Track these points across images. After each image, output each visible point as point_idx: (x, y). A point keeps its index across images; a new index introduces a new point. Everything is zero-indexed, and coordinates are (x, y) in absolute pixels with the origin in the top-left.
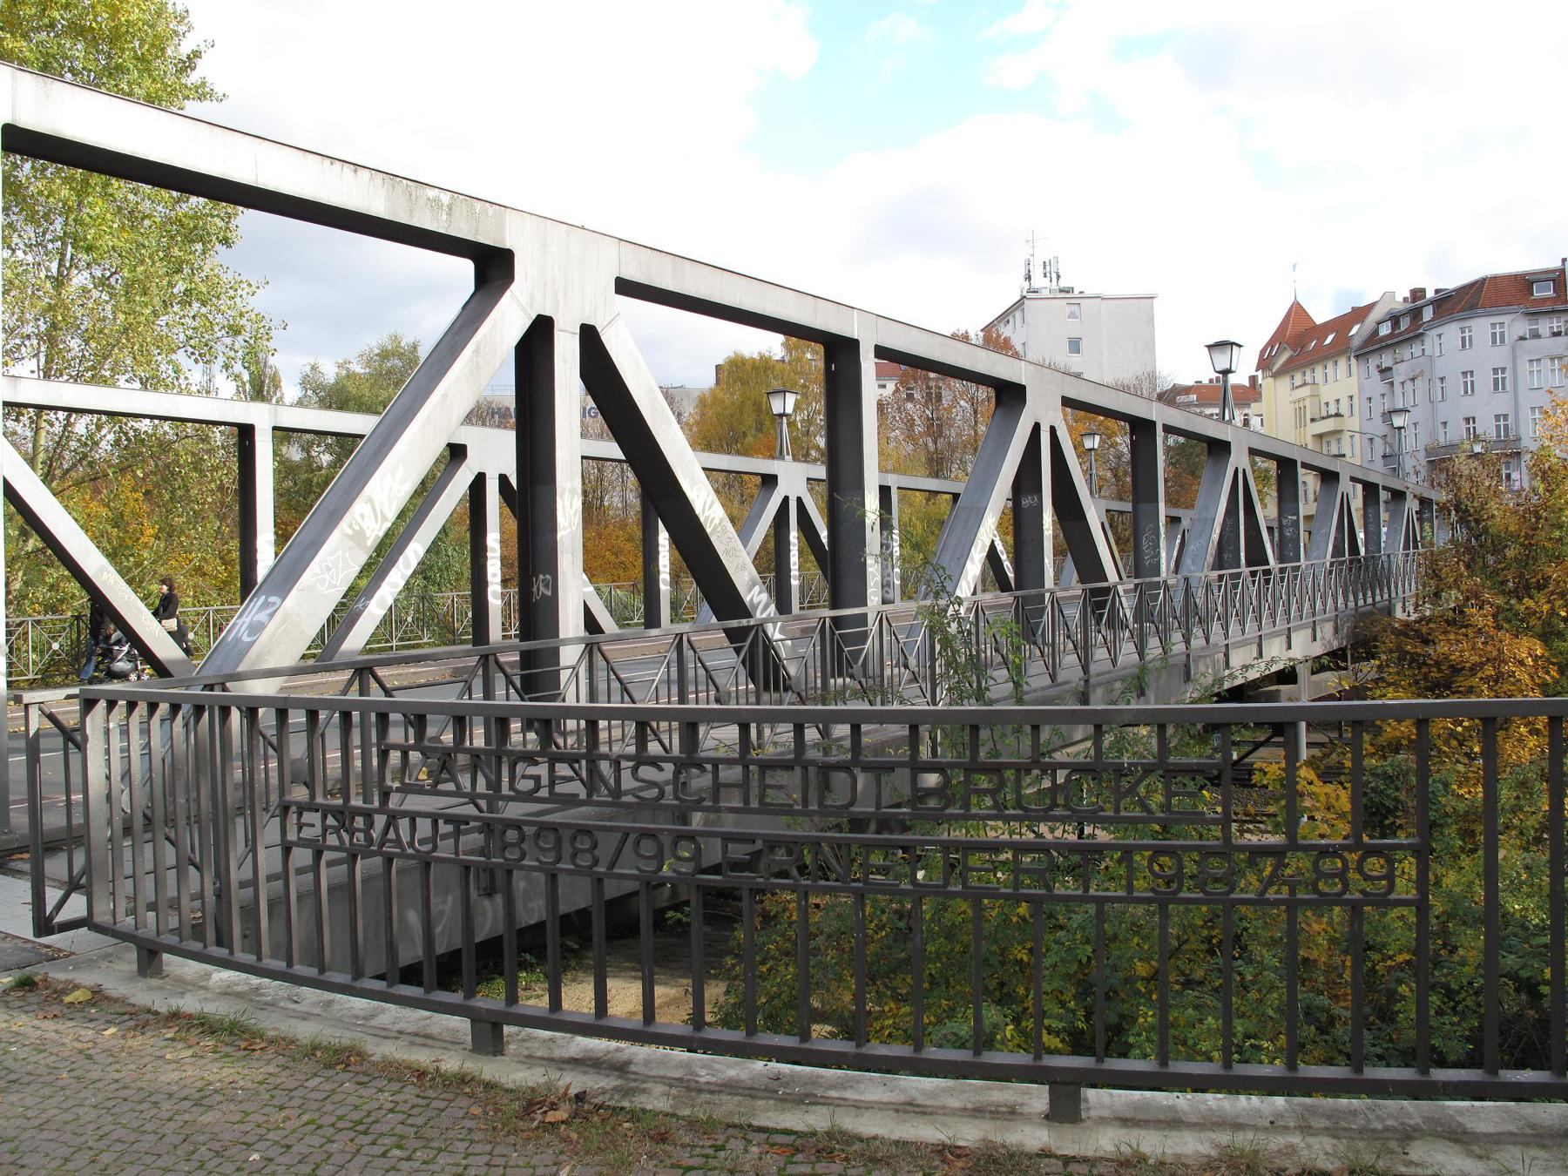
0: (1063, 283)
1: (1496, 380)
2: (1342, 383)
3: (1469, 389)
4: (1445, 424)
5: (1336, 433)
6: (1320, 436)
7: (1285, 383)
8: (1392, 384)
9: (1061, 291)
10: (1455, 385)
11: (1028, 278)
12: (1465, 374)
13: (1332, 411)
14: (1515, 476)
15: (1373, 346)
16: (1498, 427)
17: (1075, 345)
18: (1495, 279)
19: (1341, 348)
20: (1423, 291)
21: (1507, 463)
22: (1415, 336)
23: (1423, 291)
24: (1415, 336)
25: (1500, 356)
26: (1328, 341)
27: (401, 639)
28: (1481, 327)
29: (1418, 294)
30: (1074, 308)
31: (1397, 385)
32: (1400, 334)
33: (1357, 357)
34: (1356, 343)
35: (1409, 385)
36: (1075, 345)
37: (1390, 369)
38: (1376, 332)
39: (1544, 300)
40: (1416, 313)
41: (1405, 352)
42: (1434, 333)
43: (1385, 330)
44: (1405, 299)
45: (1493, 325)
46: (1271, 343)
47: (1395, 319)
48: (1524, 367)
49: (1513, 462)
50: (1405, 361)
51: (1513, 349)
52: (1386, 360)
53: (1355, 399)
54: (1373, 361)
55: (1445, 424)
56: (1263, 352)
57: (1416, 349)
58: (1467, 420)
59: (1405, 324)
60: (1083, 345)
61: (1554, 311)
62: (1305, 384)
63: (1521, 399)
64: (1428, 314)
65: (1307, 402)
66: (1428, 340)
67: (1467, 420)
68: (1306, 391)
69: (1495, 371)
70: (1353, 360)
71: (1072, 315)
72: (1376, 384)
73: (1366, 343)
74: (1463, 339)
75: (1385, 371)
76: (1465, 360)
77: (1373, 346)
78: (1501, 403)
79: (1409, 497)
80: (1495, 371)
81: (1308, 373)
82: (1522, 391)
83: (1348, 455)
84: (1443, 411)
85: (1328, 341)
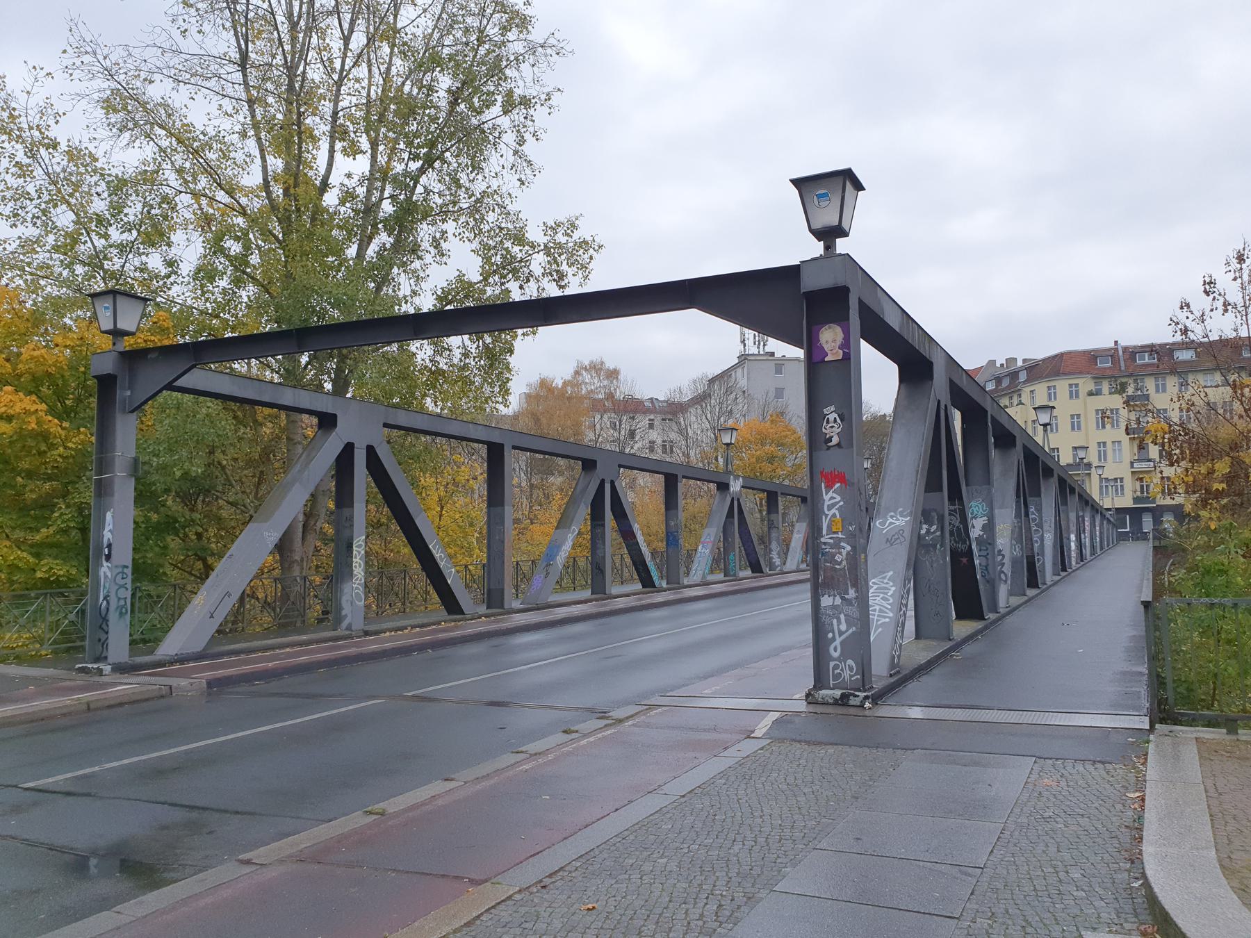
1: (1073, 424)
18: (1070, 353)
44: (1002, 365)
47: (998, 380)
60: (786, 393)
64: (1023, 376)
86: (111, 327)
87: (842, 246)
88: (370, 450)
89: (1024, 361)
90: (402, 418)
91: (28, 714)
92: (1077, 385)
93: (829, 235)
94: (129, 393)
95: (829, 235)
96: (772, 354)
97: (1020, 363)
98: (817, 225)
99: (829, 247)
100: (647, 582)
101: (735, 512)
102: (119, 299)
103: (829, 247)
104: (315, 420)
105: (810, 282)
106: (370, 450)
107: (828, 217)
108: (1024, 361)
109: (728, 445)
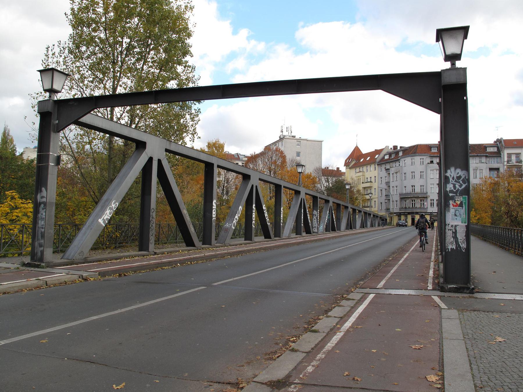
0: (293, 134)
1: (421, 175)
2: (372, 172)
3: (413, 177)
4: (405, 187)
5: (370, 187)
6: (364, 188)
7: (353, 171)
8: (389, 174)
9: (292, 137)
10: (409, 175)
11: (282, 132)
12: (412, 172)
13: (369, 180)
14: (425, 204)
15: (382, 162)
16: (421, 189)
17: (298, 154)
18: (420, 145)
19: (373, 161)
20: (397, 146)
21: (423, 200)
22: (397, 160)
23: (397, 146)
24: (397, 160)
25: (422, 168)
26: (362, 160)
27: (119, 244)
28: (417, 159)
29: (395, 147)
30: (298, 143)
31: (391, 175)
32: (392, 159)
33: (378, 165)
34: (378, 160)
35: (395, 175)
36: (298, 154)
37: (389, 169)
38: (384, 157)
39: (435, 153)
40: (397, 153)
41: (394, 164)
42: (403, 159)
43: (387, 157)
44: (391, 149)
45: (421, 159)
46: (349, 158)
47: (390, 154)
48: (429, 172)
49: (425, 200)
50: (394, 168)
51: (426, 167)
52: (388, 167)
53: (377, 177)
54: (383, 167)
55: (405, 187)
56: (346, 161)
57: (397, 164)
58: (412, 186)
59: (393, 156)
60: (301, 154)
61: (477, 156)
62: (360, 172)
63: (428, 182)
64: (401, 154)
65: (361, 177)
66: (401, 161)
67: (412, 186)
68: (361, 174)
69: (421, 172)
70: (377, 166)
71: (298, 145)
72: (384, 173)
73: (381, 161)
74: (412, 162)
75: (387, 170)
76: (412, 169)
77: (382, 162)
78: (422, 182)
79: (349, 208)
80: (421, 172)
81: (361, 168)
82: (428, 179)
83: (374, 194)
84: (405, 183)
85: (362, 160)
86: (50, 87)
87: (459, 64)
88: (159, 161)
89: (401, 147)
90: (173, 148)
91: (58, 280)
92: (423, 159)
93: (453, 58)
94: (57, 122)
95: (453, 58)
96: (294, 137)
97: (399, 148)
98: (448, 52)
99: (453, 64)
100: (190, 243)
101: (302, 205)
102: (56, 74)
103: (453, 64)
104: (134, 145)
105: (446, 80)
106: (159, 161)
107: (452, 49)
108: (401, 147)
109: (300, 173)
